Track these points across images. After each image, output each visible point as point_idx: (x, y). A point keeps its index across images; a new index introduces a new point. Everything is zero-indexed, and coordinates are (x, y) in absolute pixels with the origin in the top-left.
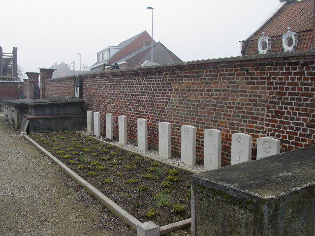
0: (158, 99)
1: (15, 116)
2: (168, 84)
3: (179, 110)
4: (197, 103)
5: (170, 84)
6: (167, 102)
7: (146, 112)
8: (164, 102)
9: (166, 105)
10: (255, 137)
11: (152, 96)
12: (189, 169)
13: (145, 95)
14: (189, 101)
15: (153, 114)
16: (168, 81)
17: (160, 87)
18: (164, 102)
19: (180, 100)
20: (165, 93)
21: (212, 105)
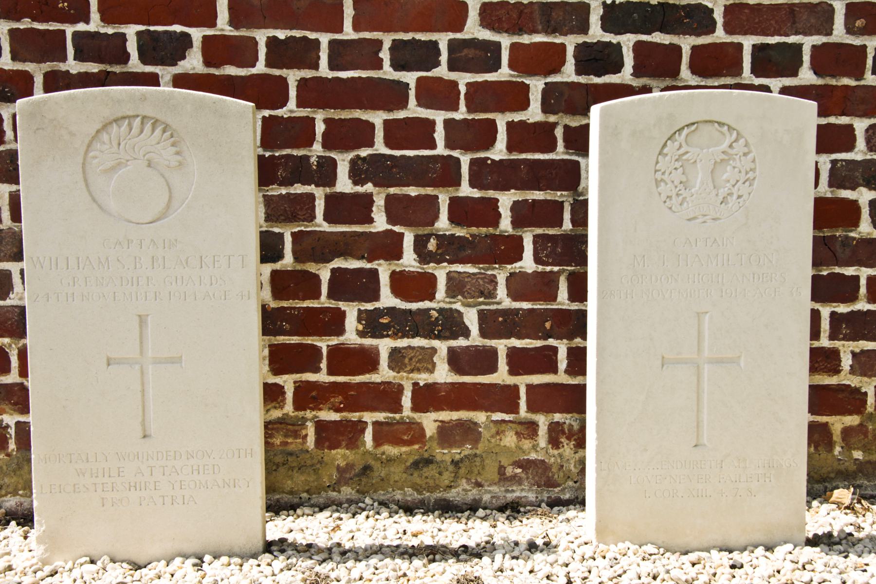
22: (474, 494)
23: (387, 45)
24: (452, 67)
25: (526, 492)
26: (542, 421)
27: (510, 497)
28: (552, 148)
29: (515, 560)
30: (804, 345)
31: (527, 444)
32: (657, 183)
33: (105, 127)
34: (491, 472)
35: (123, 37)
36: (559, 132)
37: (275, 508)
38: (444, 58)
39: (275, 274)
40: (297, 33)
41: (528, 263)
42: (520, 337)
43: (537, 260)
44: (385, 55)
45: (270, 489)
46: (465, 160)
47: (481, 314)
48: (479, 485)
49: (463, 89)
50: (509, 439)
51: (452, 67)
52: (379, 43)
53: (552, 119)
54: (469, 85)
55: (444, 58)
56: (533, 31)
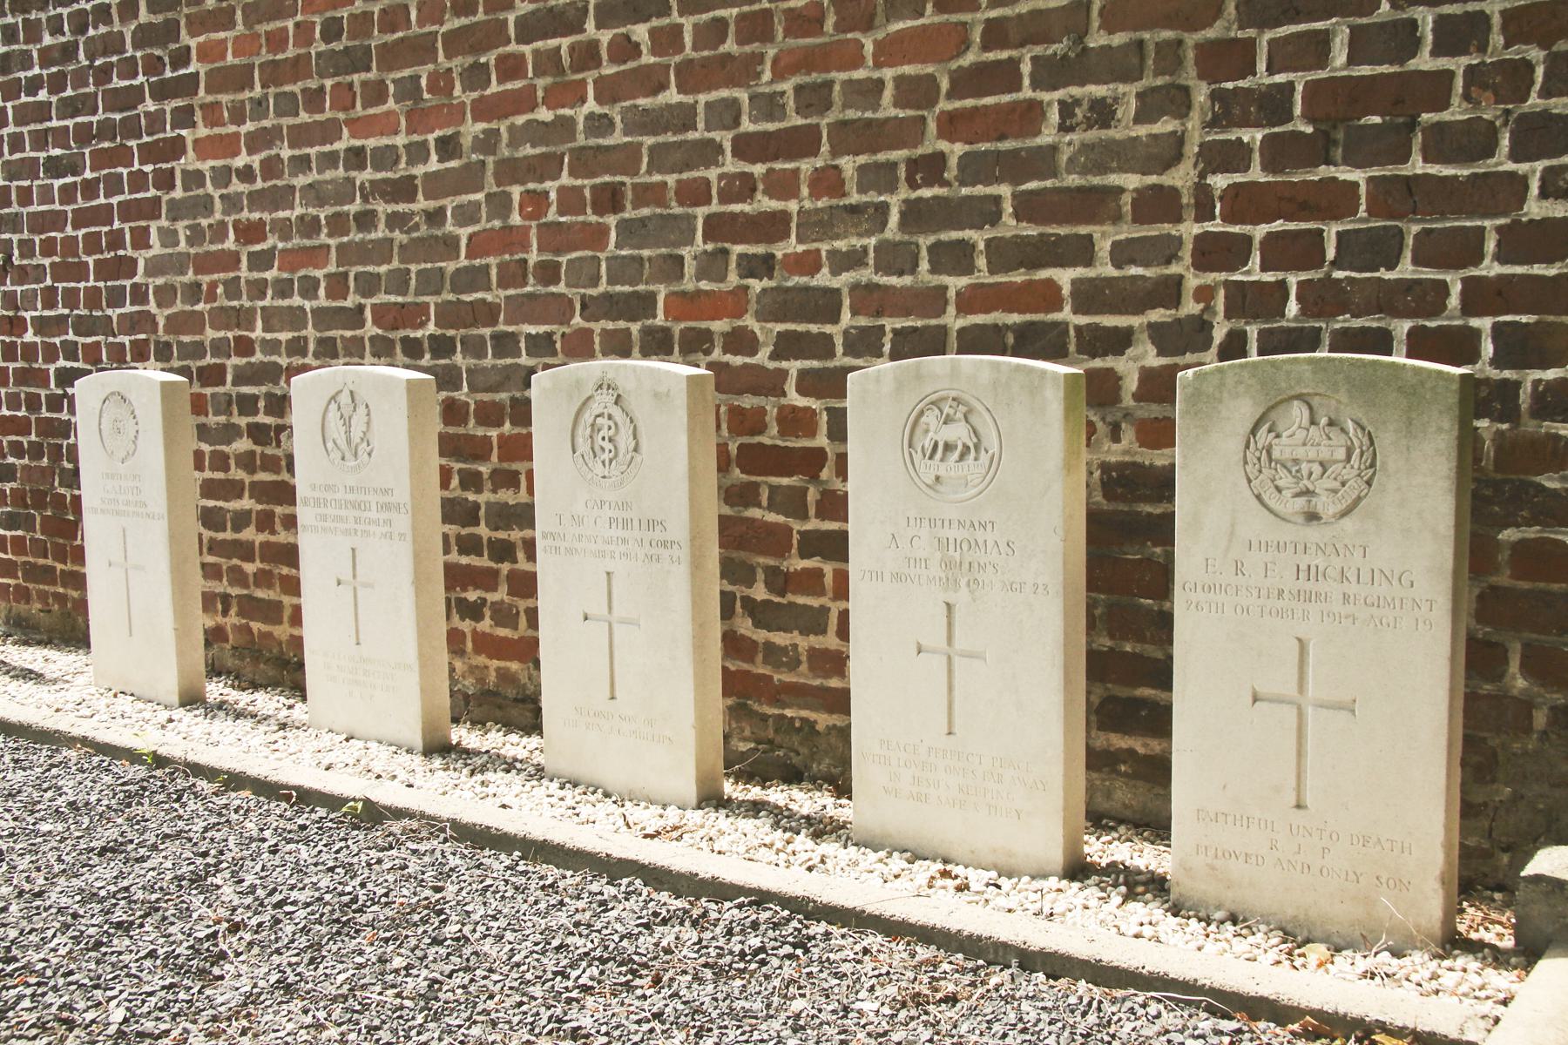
3: (261, 261)
8: (128, 211)
9: (141, 240)
15: (29, 336)
19: (271, 167)
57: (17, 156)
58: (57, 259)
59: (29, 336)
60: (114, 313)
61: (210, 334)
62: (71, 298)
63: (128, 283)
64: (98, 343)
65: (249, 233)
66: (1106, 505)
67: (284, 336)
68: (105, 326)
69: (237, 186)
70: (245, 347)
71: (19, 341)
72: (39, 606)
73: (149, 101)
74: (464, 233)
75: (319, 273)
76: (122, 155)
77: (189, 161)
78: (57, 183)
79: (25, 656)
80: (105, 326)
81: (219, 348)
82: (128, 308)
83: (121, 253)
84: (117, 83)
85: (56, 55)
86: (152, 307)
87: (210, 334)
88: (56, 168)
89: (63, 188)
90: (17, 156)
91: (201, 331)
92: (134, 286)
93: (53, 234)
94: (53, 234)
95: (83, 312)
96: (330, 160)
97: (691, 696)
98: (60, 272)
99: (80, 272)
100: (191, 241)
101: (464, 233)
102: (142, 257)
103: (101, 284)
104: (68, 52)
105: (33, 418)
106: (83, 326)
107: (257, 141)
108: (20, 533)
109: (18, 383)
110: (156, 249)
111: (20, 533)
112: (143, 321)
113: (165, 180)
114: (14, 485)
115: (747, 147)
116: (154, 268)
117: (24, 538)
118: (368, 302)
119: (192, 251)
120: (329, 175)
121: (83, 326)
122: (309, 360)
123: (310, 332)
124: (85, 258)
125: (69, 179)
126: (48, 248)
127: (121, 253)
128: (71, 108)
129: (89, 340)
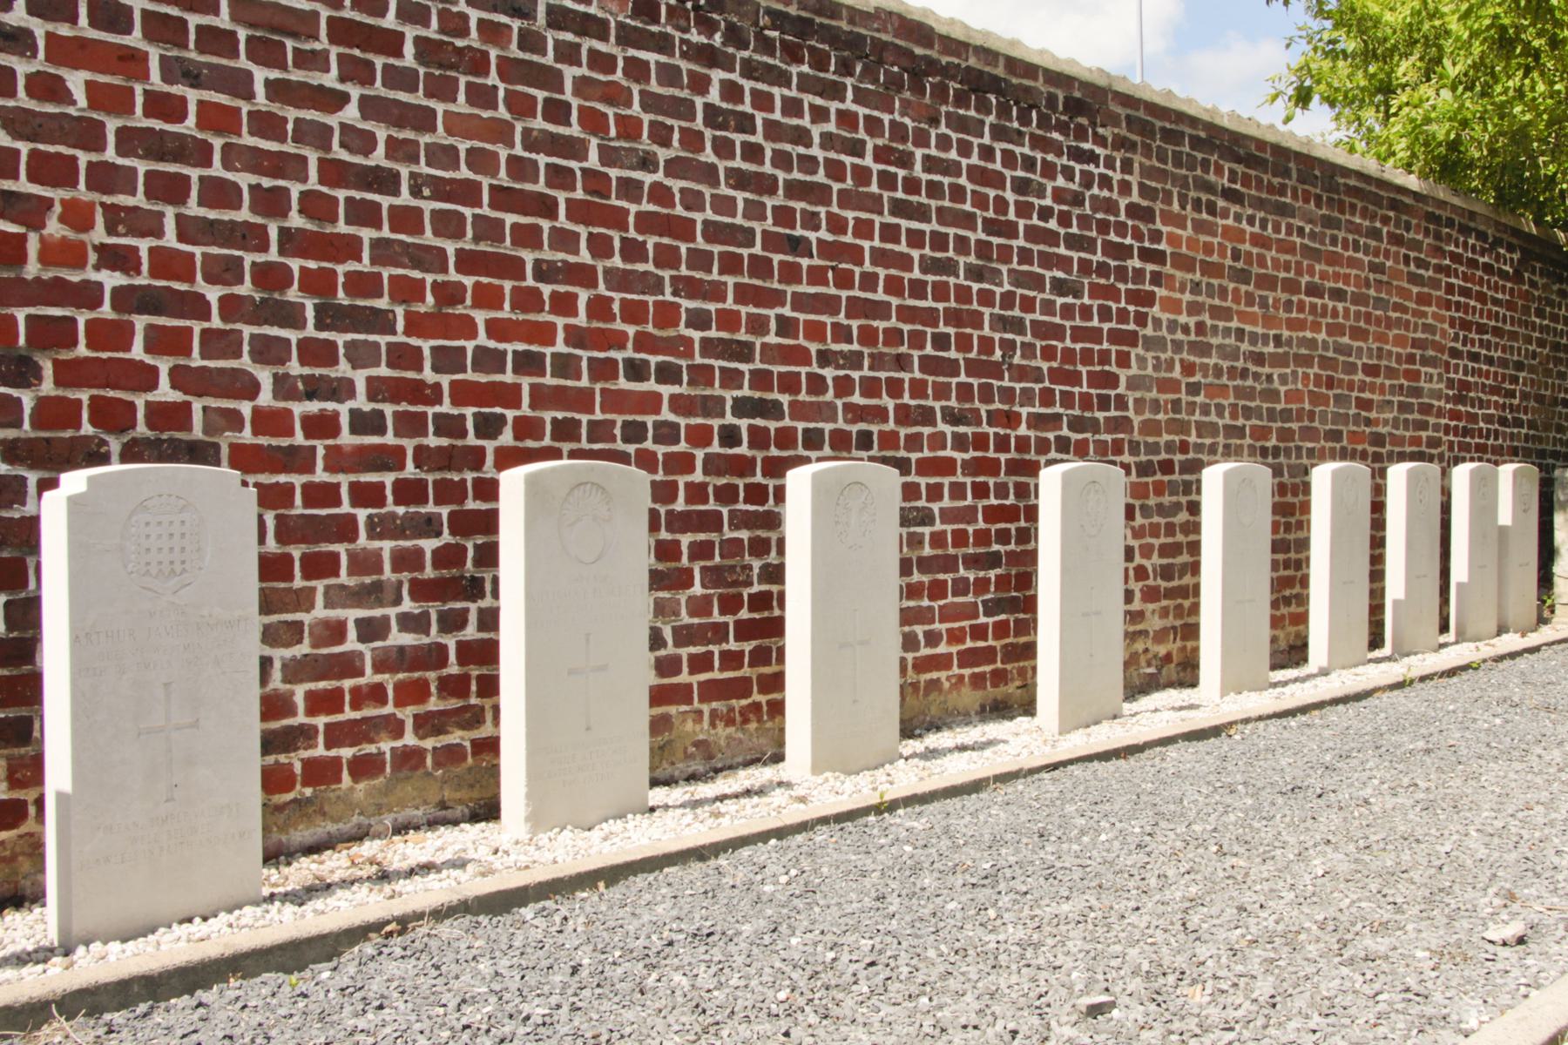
0: (1067, 311)
1: (326, 808)
2: (1133, 210)
3: (1194, 389)
4: (1270, 349)
5: (1146, 215)
6: (1131, 339)
7: (952, 418)
8: (1115, 337)
9: (1123, 361)
10: (1546, 470)
11: (1019, 279)
12: (23, 24)
13: (948, 267)
14: (1240, 334)
15: (1023, 430)
16: (1135, 197)
17: (1084, 221)
18: (1115, 337)
19: (1200, 327)
20: (1087, 356)
21: (1325, 363)
22: (669, 770)
23: (619, 424)
24: (655, 442)
25: (697, 766)
26: (706, 708)
27: (690, 770)
28: (706, 501)
29: (186, 925)
30: (254, 693)
31: (698, 728)
32: (837, 523)
33: (572, 489)
34: (680, 754)
35: (463, 417)
36: (710, 490)
37: (655, 783)
38: (650, 434)
39: (908, 585)
40: (569, 415)
41: (697, 589)
42: (695, 645)
43: (704, 586)
44: (618, 431)
45: (652, 769)
46: (725, 511)
47: (674, 629)
48: (673, 764)
49: (660, 457)
50: (689, 725)
51: (655, 442)
52: (613, 423)
53: (708, 479)
54: (665, 455)
55: (650, 434)
56: (696, 415)
57: (1025, 268)
58: (1055, 365)
59: (1023, 430)
60: (1100, 415)
61: (1166, 437)
62: (1067, 400)
63: (1113, 393)
64: (1086, 440)
65: (1188, 369)
66: (661, 567)
67: (1208, 441)
68: (1094, 426)
69: (1179, 336)
70: (1184, 446)
71: (1013, 434)
72: (1018, 683)
73: (1136, 260)
74: (1283, 389)
75: (1225, 403)
76: (1112, 293)
77: (1156, 310)
78: (1060, 301)
79: (329, 865)
80: (1094, 426)
81: (1170, 447)
82: (1113, 413)
83: (1107, 368)
84: (1113, 237)
85: (1069, 198)
86: (1131, 414)
87: (1166, 437)
88: (1060, 287)
89: (1064, 306)
90: (1025, 268)
91: (1160, 435)
92: (1118, 396)
93: (1054, 343)
94: (1054, 343)
95: (1077, 412)
96: (1227, 332)
97: (809, 723)
98: (1057, 376)
99: (1074, 379)
100: (1156, 368)
101: (1283, 389)
102: (1123, 375)
103: (1093, 391)
104: (1077, 200)
105: (725, 511)
106: (1077, 424)
107: (1194, 308)
108: (1003, 617)
109: (1008, 473)
110: (1134, 370)
111: (1003, 617)
112: (1122, 424)
113: (1141, 319)
114: (999, 571)
115: (513, 268)
116: (1133, 384)
117: (1007, 622)
118: (1248, 423)
119: (1155, 375)
120: (1227, 341)
121: (1077, 424)
122: (801, 451)
123: (1221, 440)
124: (1080, 367)
125: (1070, 300)
126: (1049, 353)
127: (1107, 368)
128: (1074, 242)
129: (1080, 436)
